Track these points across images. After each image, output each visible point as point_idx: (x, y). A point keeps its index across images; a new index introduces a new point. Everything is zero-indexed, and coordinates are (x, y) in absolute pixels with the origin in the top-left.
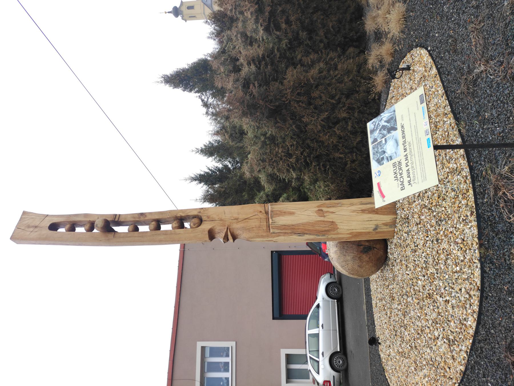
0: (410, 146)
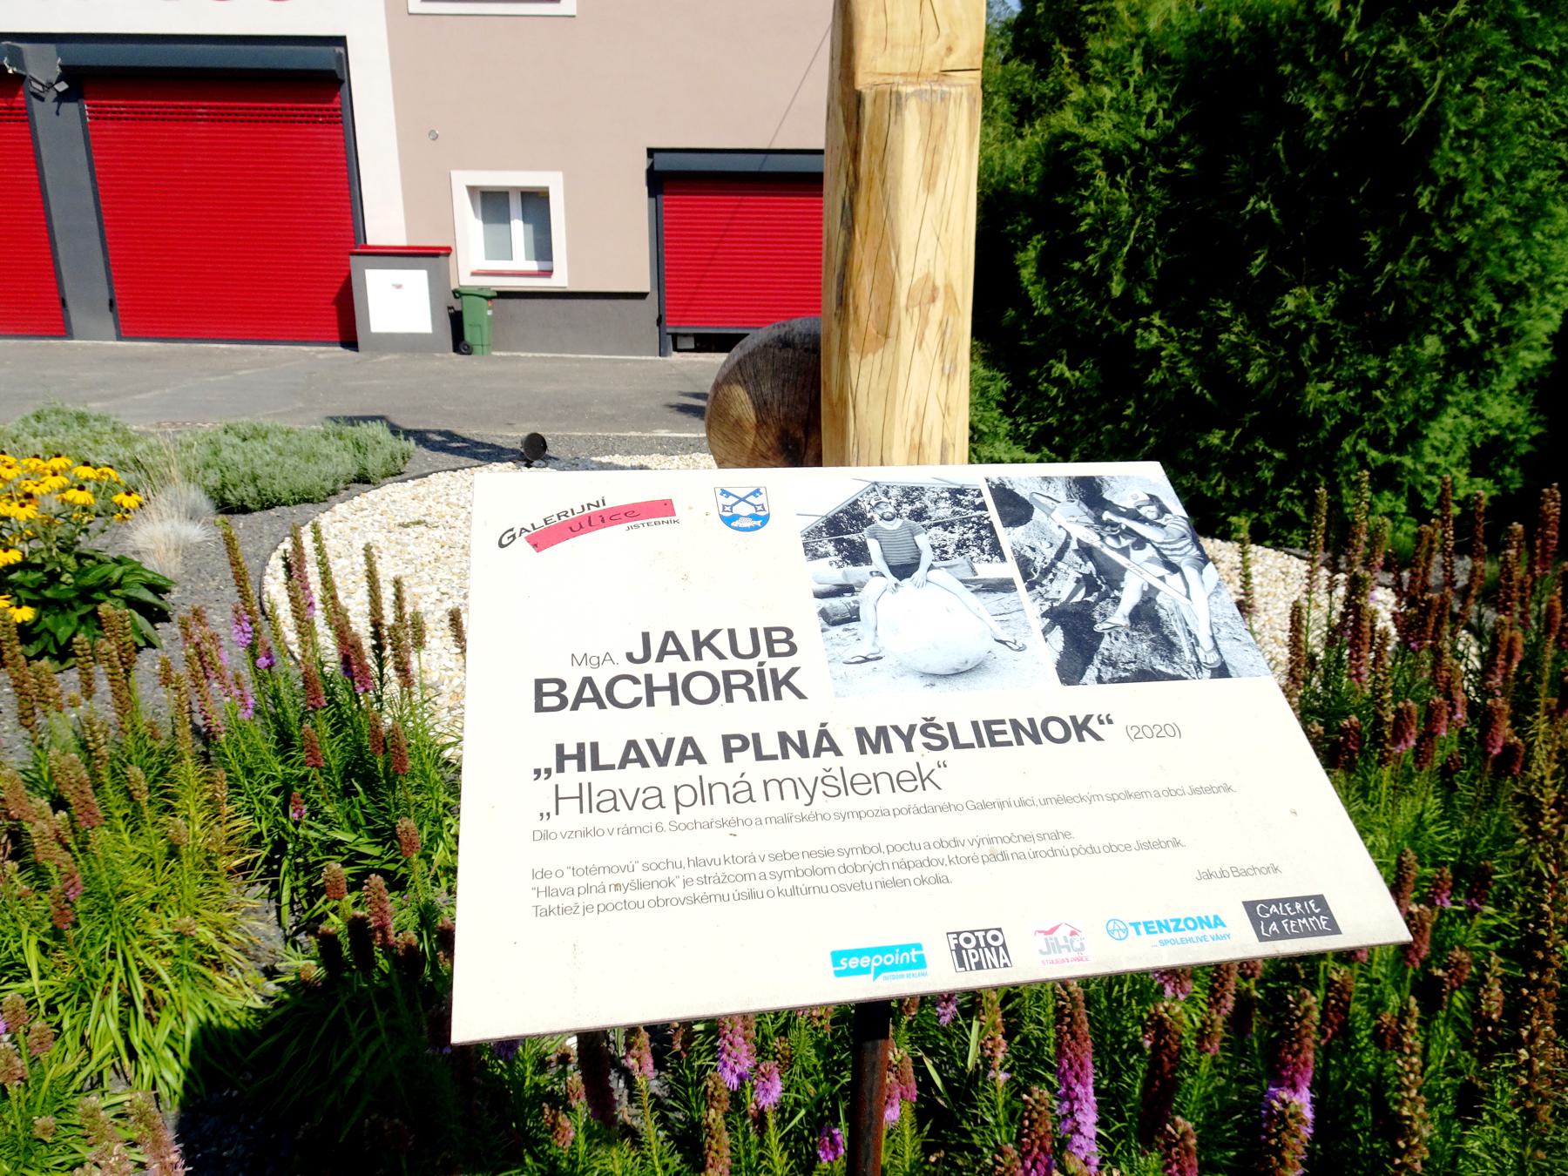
0: (896, 783)
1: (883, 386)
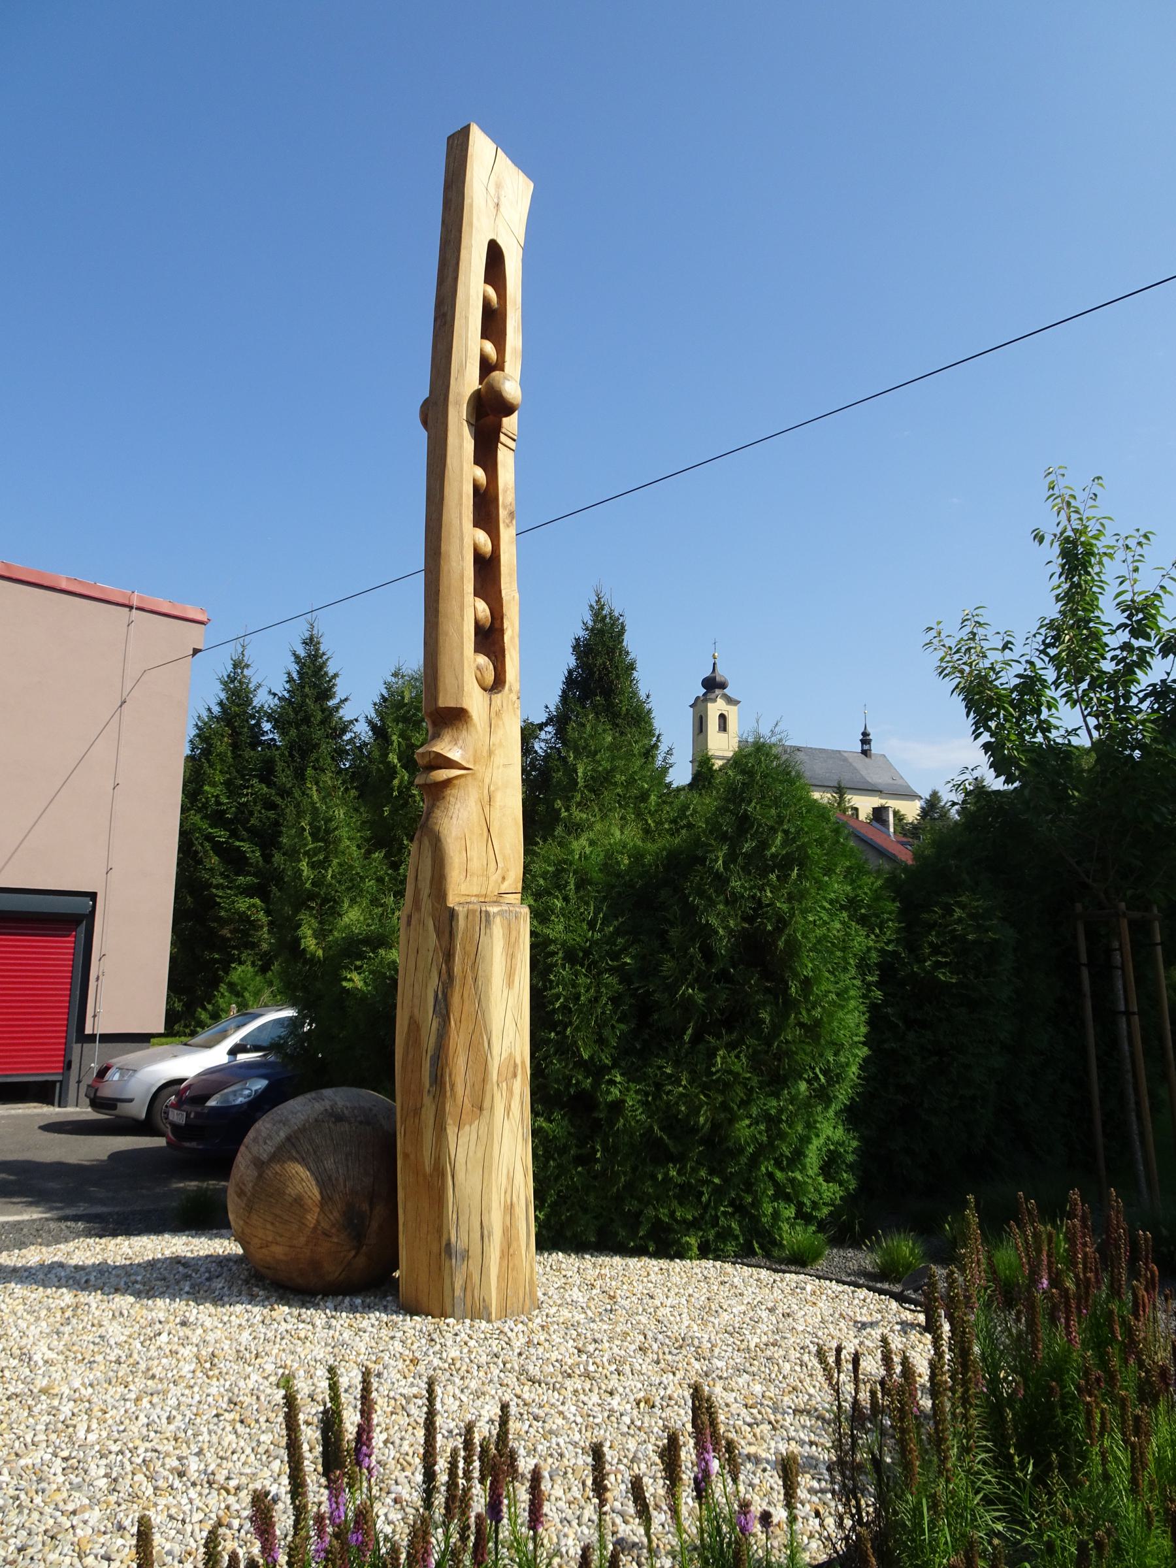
1: (480, 1155)
